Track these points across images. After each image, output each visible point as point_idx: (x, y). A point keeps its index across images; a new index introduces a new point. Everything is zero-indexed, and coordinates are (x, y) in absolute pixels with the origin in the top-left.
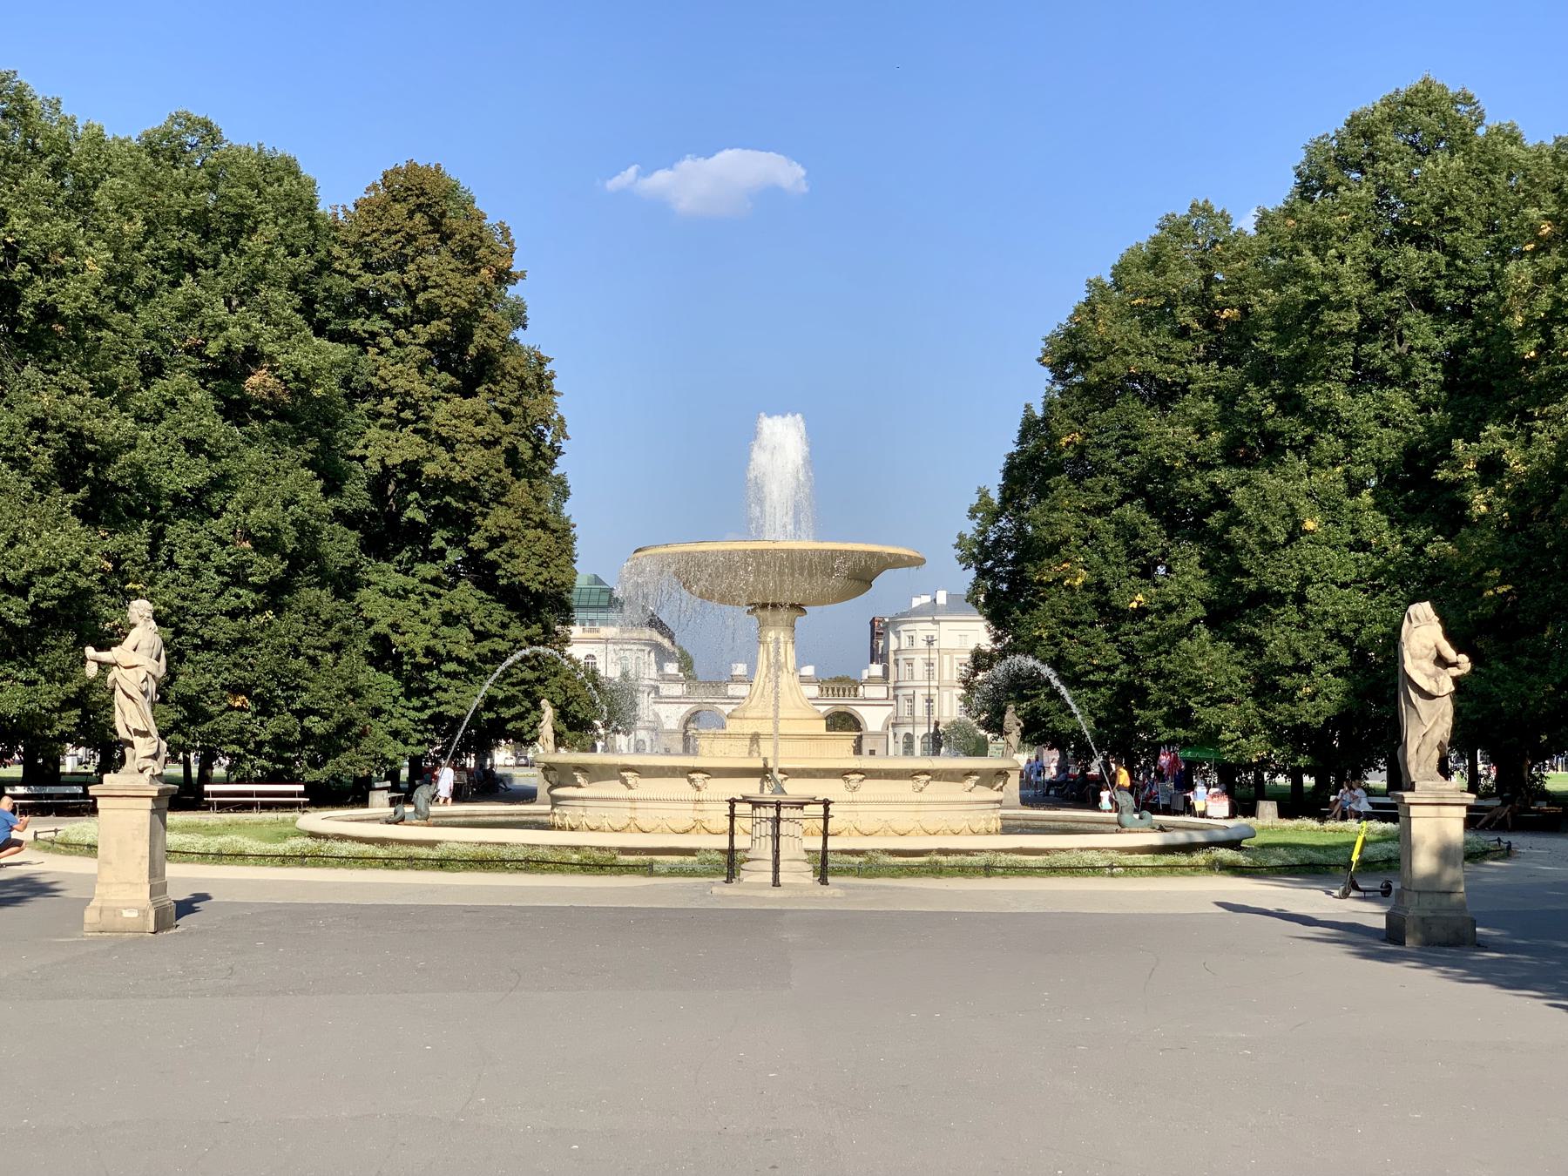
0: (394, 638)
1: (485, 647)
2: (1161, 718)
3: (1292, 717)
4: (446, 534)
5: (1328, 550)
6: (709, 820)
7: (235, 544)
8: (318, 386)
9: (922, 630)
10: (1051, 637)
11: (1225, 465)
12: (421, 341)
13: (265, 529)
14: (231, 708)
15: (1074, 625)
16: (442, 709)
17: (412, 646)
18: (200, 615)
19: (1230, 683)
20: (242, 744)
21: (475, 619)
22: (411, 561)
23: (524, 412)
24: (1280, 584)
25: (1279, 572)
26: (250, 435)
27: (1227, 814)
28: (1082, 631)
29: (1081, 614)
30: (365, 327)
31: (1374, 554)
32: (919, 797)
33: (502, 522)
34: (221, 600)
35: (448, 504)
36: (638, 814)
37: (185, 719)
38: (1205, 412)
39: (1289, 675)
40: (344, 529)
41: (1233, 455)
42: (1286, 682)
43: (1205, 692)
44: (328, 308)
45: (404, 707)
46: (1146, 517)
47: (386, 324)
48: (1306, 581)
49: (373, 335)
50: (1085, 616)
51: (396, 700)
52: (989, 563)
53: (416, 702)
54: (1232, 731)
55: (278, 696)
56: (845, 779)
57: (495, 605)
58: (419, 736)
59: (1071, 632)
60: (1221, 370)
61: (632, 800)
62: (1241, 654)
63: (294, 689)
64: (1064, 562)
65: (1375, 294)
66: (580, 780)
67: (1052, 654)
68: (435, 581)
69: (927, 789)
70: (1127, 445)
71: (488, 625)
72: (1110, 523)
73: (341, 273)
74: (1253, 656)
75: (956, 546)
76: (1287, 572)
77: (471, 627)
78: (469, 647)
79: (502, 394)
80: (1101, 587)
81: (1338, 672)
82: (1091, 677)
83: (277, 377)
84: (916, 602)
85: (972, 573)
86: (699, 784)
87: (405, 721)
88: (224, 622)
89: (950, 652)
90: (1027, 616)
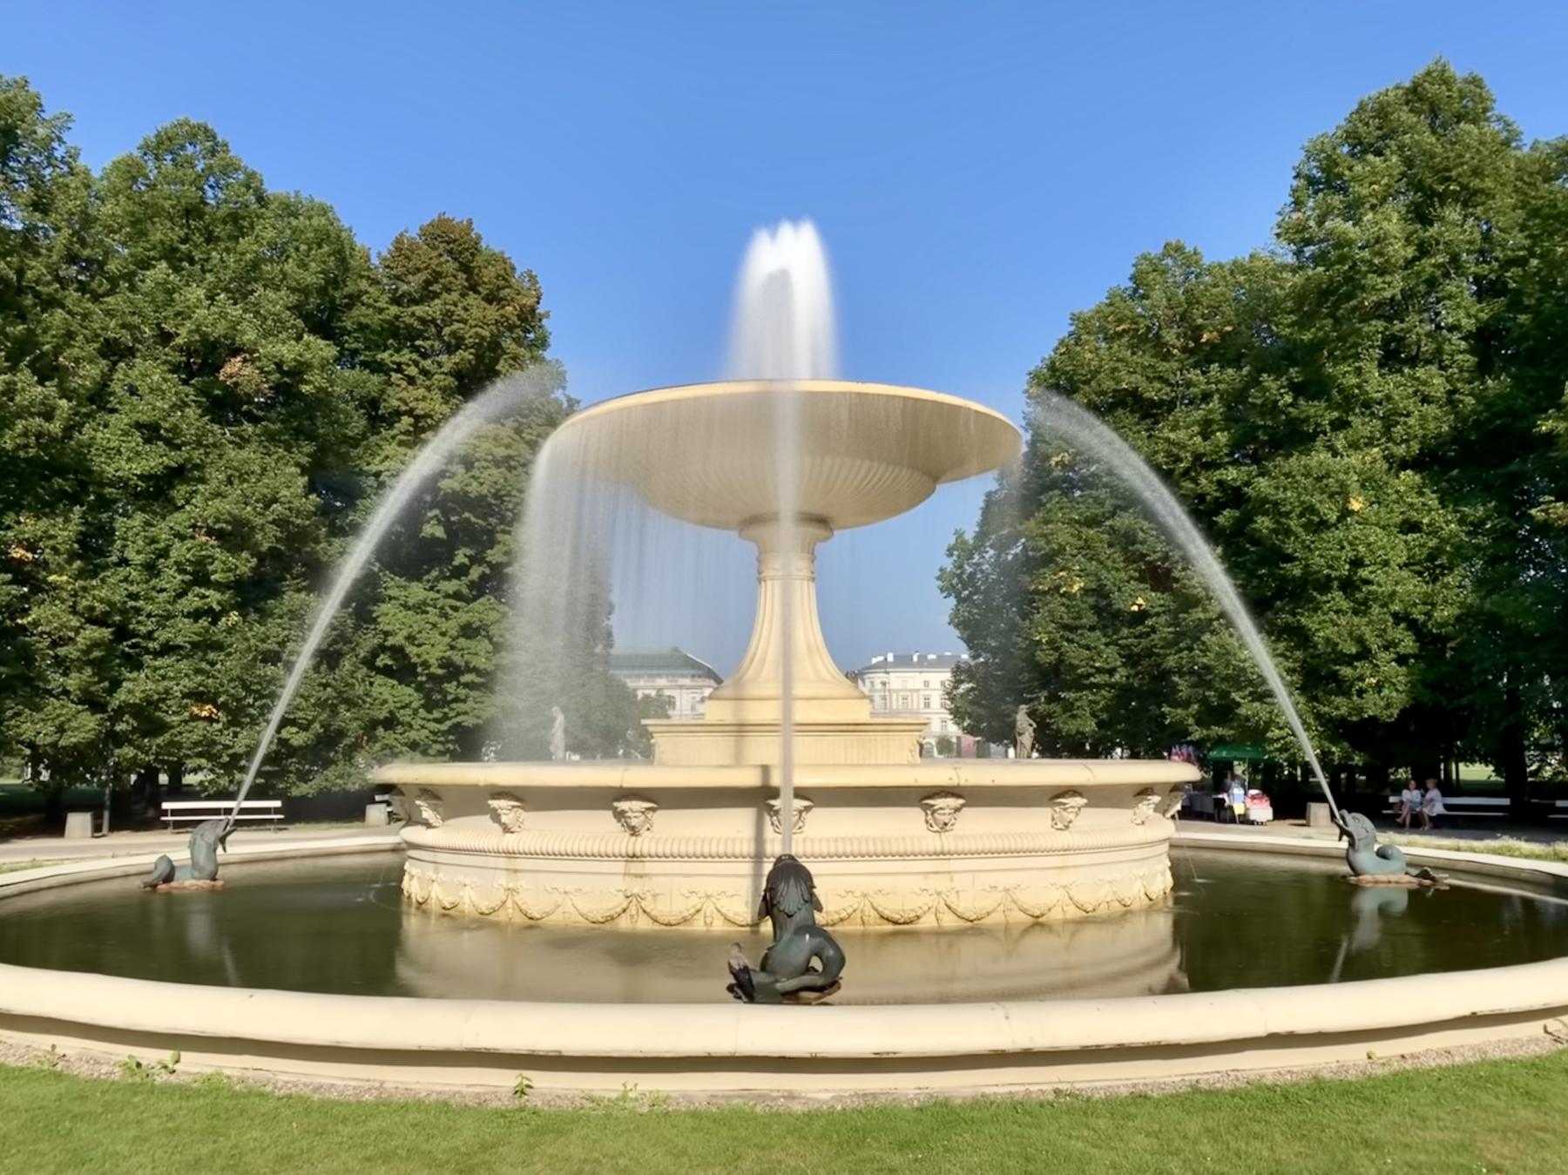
0: (411, 650)
2: (1193, 716)
4: (469, 552)
5: (1378, 530)
6: (655, 896)
7: (193, 537)
8: (307, 382)
9: (878, 677)
10: (1051, 642)
12: (445, 370)
15: (1072, 629)
16: (459, 719)
17: (425, 657)
22: (437, 579)
24: (1330, 567)
25: (1325, 555)
26: (241, 437)
27: (1271, 817)
29: (1080, 618)
32: (1063, 840)
34: (183, 601)
35: (467, 520)
36: (522, 882)
37: (134, 730)
38: (1210, 411)
39: (1350, 664)
42: (1346, 671)
43: (1246, 687)
44: (357, 340)
45: (423, 719)
47: (415, 356)
48: (1357, 563)
49: (399, 364)
50: (1084, 621)
51: (415, 712)
53: (437, 714)
54: (1281, 729)
55: (250, 705)
56: (926, 808)
58: (439, 747)
59: (1071, 636)
61: (510, 854)
65: (1030, 572)
66: (427, 814)
67: (1052, 658)
68: (457, 596)
72: (1102, 533)
73: (369, 306)
74: (1297, 647)
75: (939, 578)
76: (1338, 554)
78: (487, 659)
79: (530, 427)
80: (1100, 592)
81: (1401, 660)
82: (1092, 679)
83: (258, 368)
84: (874, 661)
85: (952, 601)
86: (634, 822)
87: (426, 732)
88: (185, 624)
89: (897, 691)
90: (1027, 622)
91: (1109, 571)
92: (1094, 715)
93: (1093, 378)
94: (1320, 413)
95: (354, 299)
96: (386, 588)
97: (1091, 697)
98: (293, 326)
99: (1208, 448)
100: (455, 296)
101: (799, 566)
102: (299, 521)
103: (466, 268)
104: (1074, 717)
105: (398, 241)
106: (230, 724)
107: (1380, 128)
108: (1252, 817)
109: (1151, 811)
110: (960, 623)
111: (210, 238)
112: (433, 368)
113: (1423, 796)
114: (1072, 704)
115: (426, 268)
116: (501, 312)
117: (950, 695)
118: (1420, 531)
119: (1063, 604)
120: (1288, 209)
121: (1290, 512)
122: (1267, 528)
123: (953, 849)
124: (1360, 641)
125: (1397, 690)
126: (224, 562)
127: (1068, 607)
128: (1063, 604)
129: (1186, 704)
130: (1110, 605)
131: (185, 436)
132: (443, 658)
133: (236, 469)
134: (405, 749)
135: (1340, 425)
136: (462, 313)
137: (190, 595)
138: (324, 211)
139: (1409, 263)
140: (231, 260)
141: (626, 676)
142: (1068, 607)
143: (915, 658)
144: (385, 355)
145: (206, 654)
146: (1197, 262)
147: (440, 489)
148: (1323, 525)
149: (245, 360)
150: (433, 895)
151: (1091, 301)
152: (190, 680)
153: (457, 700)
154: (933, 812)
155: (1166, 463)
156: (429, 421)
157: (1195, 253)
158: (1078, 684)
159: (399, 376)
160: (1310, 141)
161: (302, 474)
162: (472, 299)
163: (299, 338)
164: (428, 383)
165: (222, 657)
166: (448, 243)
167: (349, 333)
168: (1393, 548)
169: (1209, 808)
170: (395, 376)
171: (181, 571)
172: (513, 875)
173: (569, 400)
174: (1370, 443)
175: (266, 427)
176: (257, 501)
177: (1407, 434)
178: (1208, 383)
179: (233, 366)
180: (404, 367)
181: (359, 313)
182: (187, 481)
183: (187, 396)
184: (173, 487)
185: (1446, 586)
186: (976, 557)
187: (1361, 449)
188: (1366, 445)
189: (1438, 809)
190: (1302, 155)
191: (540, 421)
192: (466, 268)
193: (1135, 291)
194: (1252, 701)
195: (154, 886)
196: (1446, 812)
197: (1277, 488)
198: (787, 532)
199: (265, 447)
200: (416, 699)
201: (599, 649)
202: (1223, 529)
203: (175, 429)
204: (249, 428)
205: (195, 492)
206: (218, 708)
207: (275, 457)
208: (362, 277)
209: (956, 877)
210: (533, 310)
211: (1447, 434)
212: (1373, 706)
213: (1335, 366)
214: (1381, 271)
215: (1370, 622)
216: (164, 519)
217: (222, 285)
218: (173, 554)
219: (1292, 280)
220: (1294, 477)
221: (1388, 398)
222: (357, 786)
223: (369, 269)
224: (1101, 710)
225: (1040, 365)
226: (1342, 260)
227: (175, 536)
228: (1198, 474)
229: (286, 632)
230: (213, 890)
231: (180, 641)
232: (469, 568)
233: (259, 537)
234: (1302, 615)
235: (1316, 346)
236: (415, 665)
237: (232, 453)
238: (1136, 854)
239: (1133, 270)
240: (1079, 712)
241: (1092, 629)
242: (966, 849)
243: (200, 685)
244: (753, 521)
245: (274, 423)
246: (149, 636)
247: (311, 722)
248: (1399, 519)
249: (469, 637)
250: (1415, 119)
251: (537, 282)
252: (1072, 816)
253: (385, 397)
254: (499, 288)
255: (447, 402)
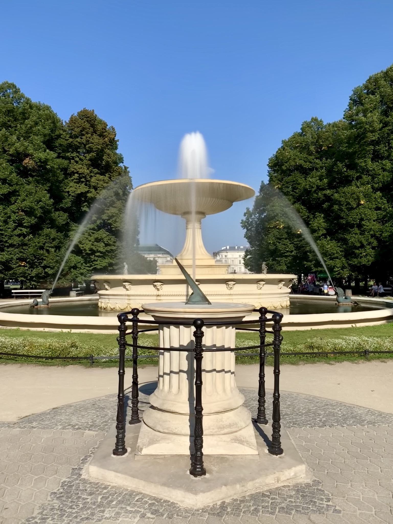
1: (109, 248)
2: (313, 265)
3: (360, 263)
7: (18, 213)
8: (48, 165)
9: (224, 254)
10: (274, 243)
11: (328, 189)
13: (27, 208)
14: (20, 266)
15: (280, 239)
16: (95, 266)
17: (85, 248)
18: (8, 236)
19: (337, 253)
20: (24, 277)
21: (105, 240)
23: (120, 181)
24: (354, 221)
25: (353, 217)
28: (283, 241)
30: (71, 155)
31: (383, 211)
32: (260, 292)
33: (112, 211)
34: (15, 231)
36: (131, 302)
38: (322, 173)
40: (63, 213)
41: (330, 186)
42: (357, 251)
43: (328, 256)
45: (84, 266)
46: (303, 207)
48: (362, 219)
49: (73, 157)
51: (82, 264)
52: (250, 227)
53: (88, 265)
54: (338, 268)
55: (36, 262)
57: (112, 236)
60: (326, 160)
61: (128, 295)
62: (339, 244)
63: (41, 259)
64: (277, 221)
66: (107, 287)
67: (274, 248)
69: (263, 288)
70: (296, 186)
71: (109, 242)
73: (63, 139)
74: (344, 244)
75: (241, 223)
76: (356, 217)
77: (104, 242)
78: (103, 248)
81: (373, 248)
82: (286, 254)
83: (34, 161)
84: (223, 248)
85: (245, 230)
86: (158, 287)
88: (16, 238)
89: (230, 258)
90: (266, 237)
91: (291, 222)
92: (286, 265)
93: (288, 161)
94: (354, 174)
95: (59, 136)
96: (72, 227)
97: (285, 259)
98: (43, 147)
99: (321, 184)
100: (89, 135)
101: (197, 225)
102: (48, 207)
103: (93, 126)
104: (280, 265)
105: (71, 118)
106: (30, 268)
107: (375, 86)
108: (330, 294)
109: (282, 286)
110: (247, 236)
111: (16, 120)
112: (83, 158)
113: (378, 287)
114: (280, 261)
115: (80, 126)
116: (104, 140)
117: (244, 259)
118: (381, 210)
119: (277, 232)
120: (347, 110)
121: (343, 204)
122: (337, 209)
123: (233, 294)
124: (361, 242)
125: (371, 257)
126: (27, 220)
127: (279, 232)
128: (277, 232)
129: (311, 261)
130: (291, 232)
131: (14, 182)
132: (90, 248)
133: (28, 192)
134: (79, 275)
135: (359, 178)
136: (92, 141)
137: (17, 229)
138: (48, 108)
139: (380, 129)
140: (23, 127)
141: (144, 254)
142: (279, 232)
143: (236, 248)
144: (69, 154)
145: (23, 247)
146: (321, 124)
147: (87, 196)
148: (352, 208)
149: (30, 159)
150: (108, 306)
151: (287, 136)
152: (19, 255)
153: (95, 261)
154: (228, 285)
155: (309, 188)
156: (83, 175)
157: (321, 121)
158: (282, 255)
159: (73, 161)
160: (355, 88)
161: (48, 193)
162: (95, 136)
163: (45, 151)
164: (82, 163)
165: (27, 248)
166: (87, 118)
167: (57, 147)
168: (372, 215)
169: (318, 292)
170: (72, 161)
171: (14, 222)
172: (129, 300)
173: (125, 167)
174: (368, 183)
175: (36, 178)
176: (35, 201)
177: (379, 181)
178: (322, 164)
179: (27, 160)
180: (75, 158)
181: (60, 141)
182: (15, 196)
183: (12, 169)
184: (11, 197)
185: (386, 226)
186: (253, 216)
187: (365, 185)
188: (367, 184)
189: (382, 291)
190: (352, 93)
191: (117, 174)
192: (93, 126)
193: (302, 133)
194: (330, 260)
195: (34, 307)
196: (384, 292)
197: (340, 197)
198: (193, 216)
199: (36, 185)
200: (82, 261)
201: (135, 245)
202: (325, 209)
203: (11, 180)
204: (30, 179)
205: (17, 199)
206: (27, 263)
207: (39, 188)
208: (60, 129)
209: (233, 300)
210: (114, 139)
211: (390, 181)
212: (364, 261)
213: (358, 160)
214: (372, 132)
215: (364, 237)
216: (8, 207)
217: (21, 135)
218: (12, 217)
219: (347, 133)
220: (345, 193)
221: (374, 170)
222: (68, 285)
223: (63, 127)
224: (288, 263)
225: (273, 156)
226: (361, 128)
227: (12, 212)
228: (318, 192)
229: (45, 240)
230: (48, 308)
231: (15, 243)
232: (97, 221)
233: (37, 212)
234: (346, 235)
235: (354, 153)
236: (82, 250)
237: (27, 187)
238: (279, 296)
239: (302, 126)
240: (282, 264)
241: (286, 239)
242: (236, 294)
243: (21, 256)
244: (186, 213)
245: (38, 177)
246: (6, 242)
247: (54, 267)
248: (375, 206)
249: (97, 242)
250: (385, 83)
251: (115, 130)
252: (262, 286)
253: (69, 167)
254: (103, 132)
255: (88, 169)
